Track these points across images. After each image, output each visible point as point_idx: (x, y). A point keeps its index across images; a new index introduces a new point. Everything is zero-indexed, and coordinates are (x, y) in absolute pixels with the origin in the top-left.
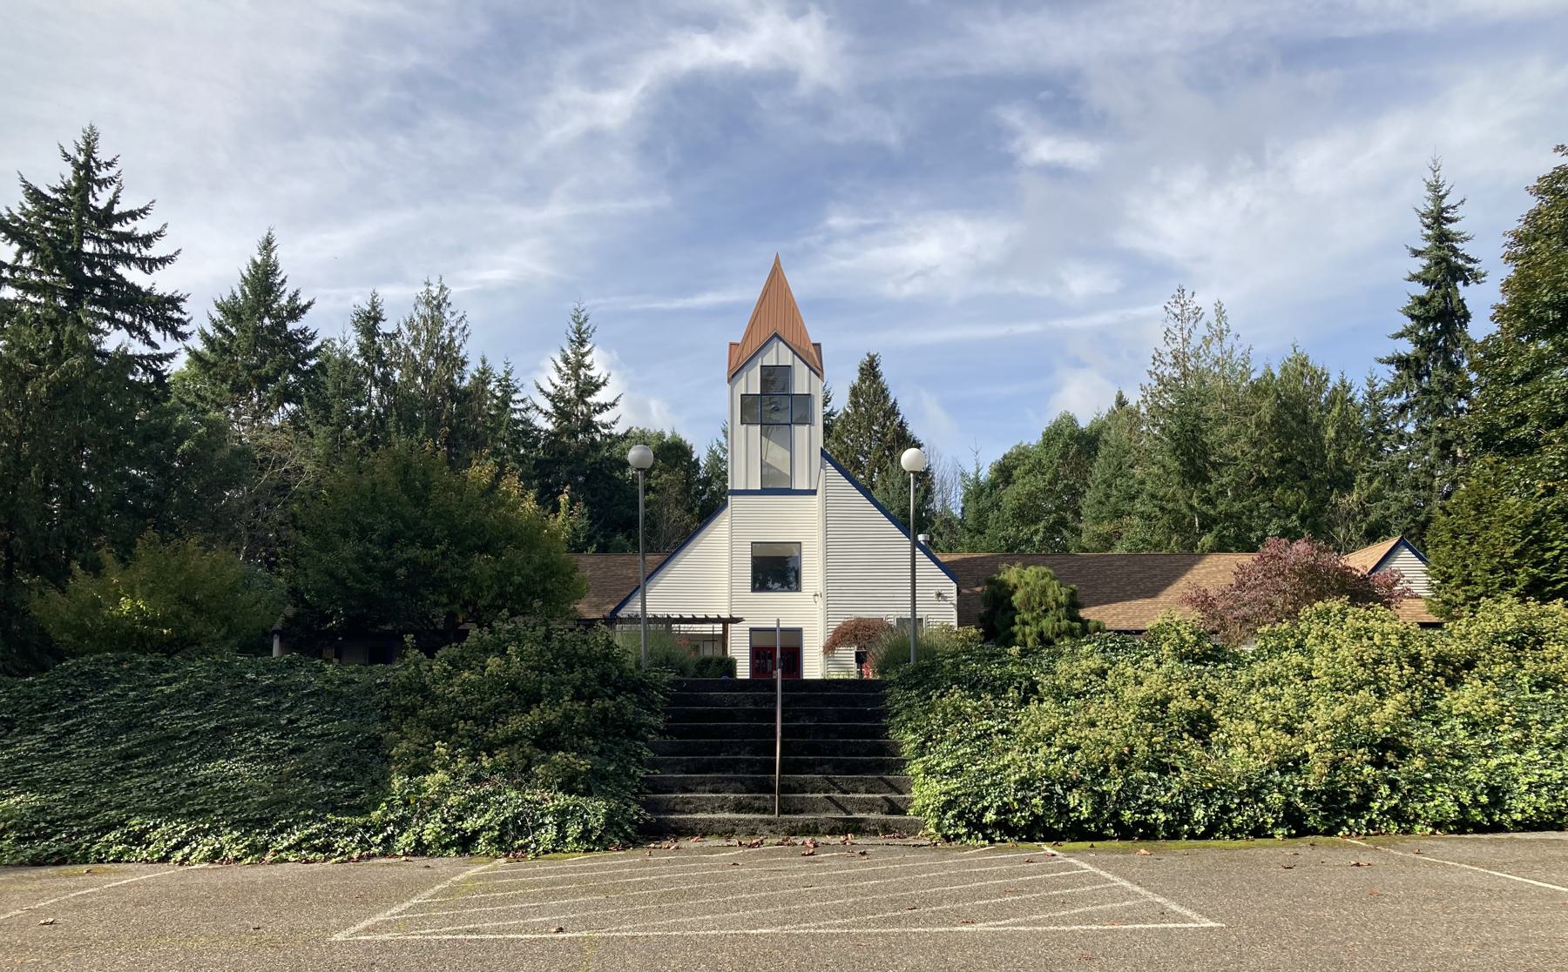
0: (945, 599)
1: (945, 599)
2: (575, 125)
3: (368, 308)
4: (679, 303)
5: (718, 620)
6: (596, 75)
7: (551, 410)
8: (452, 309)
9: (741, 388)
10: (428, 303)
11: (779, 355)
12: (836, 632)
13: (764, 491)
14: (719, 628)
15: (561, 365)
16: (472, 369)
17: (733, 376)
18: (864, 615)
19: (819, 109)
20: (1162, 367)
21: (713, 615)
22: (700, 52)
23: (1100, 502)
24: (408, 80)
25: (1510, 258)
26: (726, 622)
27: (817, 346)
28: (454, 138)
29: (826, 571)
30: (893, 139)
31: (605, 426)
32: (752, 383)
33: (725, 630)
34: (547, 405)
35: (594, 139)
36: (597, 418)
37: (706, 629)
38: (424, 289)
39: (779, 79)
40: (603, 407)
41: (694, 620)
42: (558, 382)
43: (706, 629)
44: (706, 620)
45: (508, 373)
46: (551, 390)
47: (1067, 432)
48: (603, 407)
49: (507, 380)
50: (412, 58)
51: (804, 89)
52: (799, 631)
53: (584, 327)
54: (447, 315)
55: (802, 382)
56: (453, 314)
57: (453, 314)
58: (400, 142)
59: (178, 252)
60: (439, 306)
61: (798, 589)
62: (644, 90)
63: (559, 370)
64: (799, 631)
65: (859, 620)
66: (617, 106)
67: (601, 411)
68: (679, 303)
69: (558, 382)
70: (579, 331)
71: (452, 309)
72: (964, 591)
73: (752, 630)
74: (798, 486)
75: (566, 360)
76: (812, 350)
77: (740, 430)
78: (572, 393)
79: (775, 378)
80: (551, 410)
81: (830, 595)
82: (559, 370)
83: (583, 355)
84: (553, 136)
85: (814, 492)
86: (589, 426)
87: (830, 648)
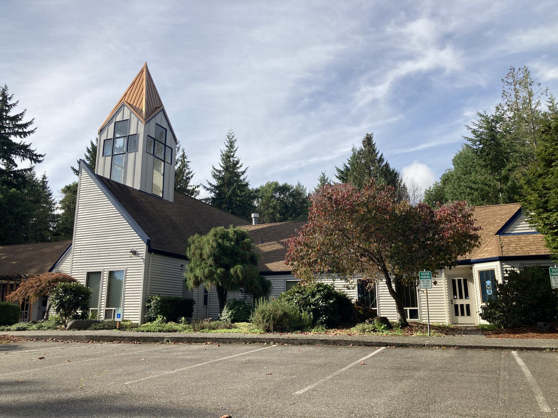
2: (368, 98)
4: (413, 149)
6: (372, 82)
16: (35, 178)
19: (454, 77)
22: (408, 68)
24: (312, 96)
25: (393, 171)
28: (328, 109)
30: (483, 83)
35: (374, 102)
39: (438, 71)
50: (315, 88)
51: (448, 71)
58: (313, 114)
59: (18, 102)
62: (390, 83)
66: (382, 90)
68: (413, 149)
84: (361, 104)
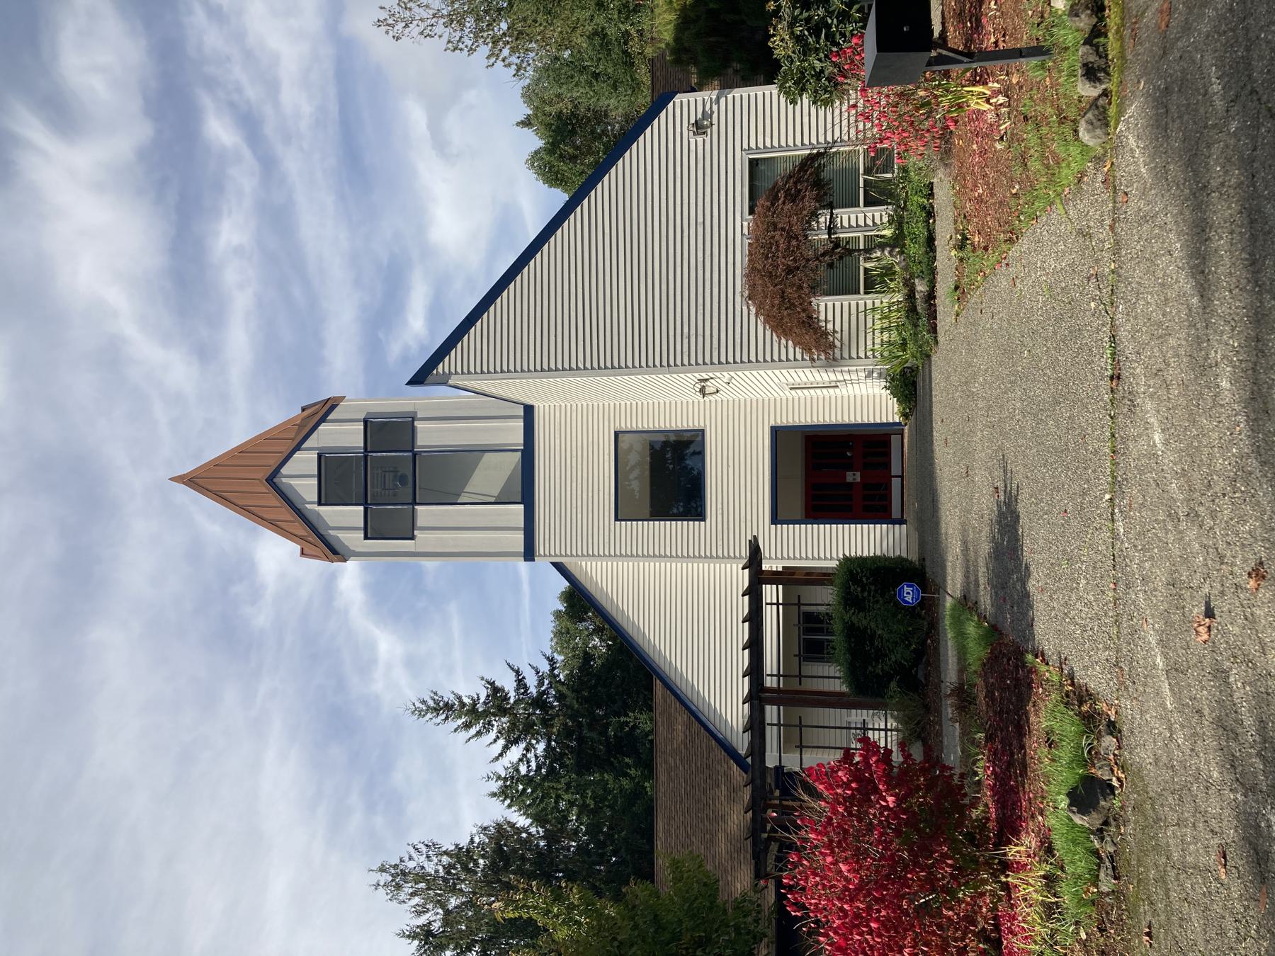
0: (707, 115)
1: (707, 115)
3: (416, 942)
5: (754, 593)
7: (523, 745)
8: (406, 859)
9: (354, 539)
10: (398, 887)
11: (301, 476)
12: (779, 326)
13: (527, 498)
14: (771, 593)
15: (473, 731)
17: (334, 552)
18: (740, 260)
20: (466, 40)
21: (744, 604)
23: (615, 88)
26: (758, 577)
27: (303, 409)
29: (650, 367)
31: (541, 683)
32: (344, 519)
33: (774, 577)
34: (516, 752)
36: (533, 691)
37: (771, 619)
38: (381, 890)
40: (521, 682)
41: (755, 645)
42: (493, 735)
43: (771, 619)
44: (755, 618)
45: (499, 778)
46: (501, 742)
47: (547, 158)
48: (521, 682)
49: (505, 779)
52: (776, 432)
53: (431, 703)
54: (411, 865)
55: (344, 435)
56: (411, 859)
57: (411, 859)
60: (404, 873)
61: (702, 432)
63: (479, 734)
64: (776, 432)
65: (752, 272)
67: (526, 688)
69: (493, 735)
70: (436, 710)
71: (406, 859)
72: (694, 80)
73: (775, 520)
74: (520, 439)
75: (467, 726)
76: (307, 412)
77: (423, 539)
78: (504, 720)
79: (337, 478)
80: (523, 745)
81: (698, 354)
82: (479, 734)
83: (463, 705)
85: (529, 411)
86: (539, 702)
87: (818, 343)
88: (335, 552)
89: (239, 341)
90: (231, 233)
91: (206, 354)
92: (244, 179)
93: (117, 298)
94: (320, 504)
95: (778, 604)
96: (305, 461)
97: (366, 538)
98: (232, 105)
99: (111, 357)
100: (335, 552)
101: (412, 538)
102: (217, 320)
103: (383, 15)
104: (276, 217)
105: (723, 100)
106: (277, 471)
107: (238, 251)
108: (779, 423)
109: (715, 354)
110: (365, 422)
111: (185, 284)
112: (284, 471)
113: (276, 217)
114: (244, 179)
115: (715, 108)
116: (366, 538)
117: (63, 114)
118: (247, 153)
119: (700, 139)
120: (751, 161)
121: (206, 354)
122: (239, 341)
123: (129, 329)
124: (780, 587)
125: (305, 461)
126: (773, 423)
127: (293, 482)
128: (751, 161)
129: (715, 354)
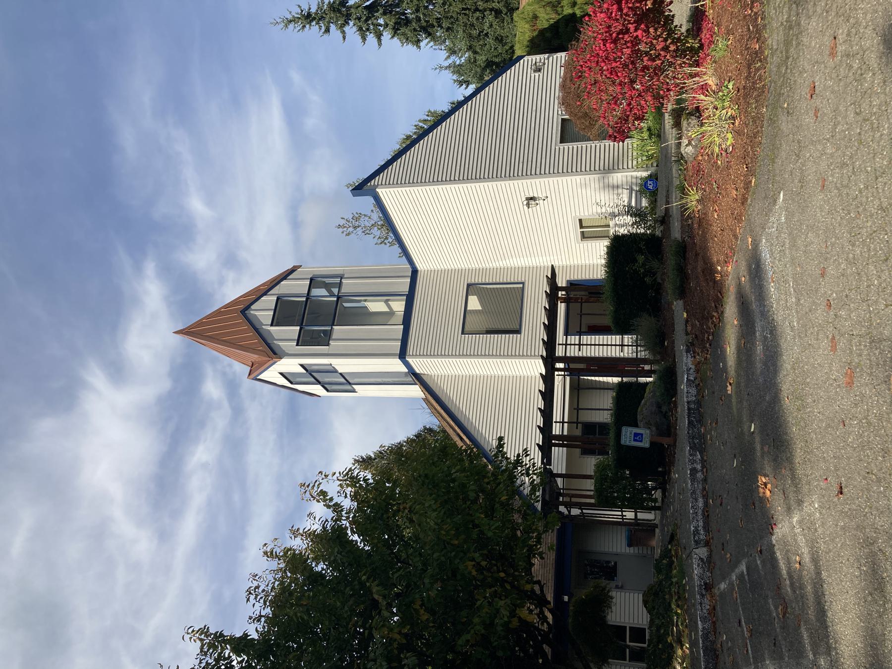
5: (548, 379)
11: (263, 311)
41: (547, 413)
44: (548, 395)
88: (275, 353)
89: (189, 527)
90: (203, 454)
91: (164, 536)
92: (220, 421)
93: (117, 490)
94: (272, 325)
95: (563, 422)
96: (269, 300)
97: (297, 345)
98: (224, 374)
99: (99, 533)
100: (275, 353)
101: (328, 345)
102: (177, 514)
103: (342, 222)
104: (235, 446)
105: (551, 59)
106: (248, 307)
107: (204, 466)
108: (572, 278)
109: (538, 170)
110: (311, 280)
111: (163, 486)
112: (253, 307)
113: (235, 446)
114: (220, 421)
115: (546, 61)
116: (297, 345)
117: (118, 371)
118: (226, 404)
119: (537, 74)
120: (562, 119)
121: (164, 536)
122: (189, 527)
123: (117, 513)
124: (568, 378)
125: (269, 300)
126: (568, 278)
127: (257, 313)
128: (562, 119)
129: (538, 170)
